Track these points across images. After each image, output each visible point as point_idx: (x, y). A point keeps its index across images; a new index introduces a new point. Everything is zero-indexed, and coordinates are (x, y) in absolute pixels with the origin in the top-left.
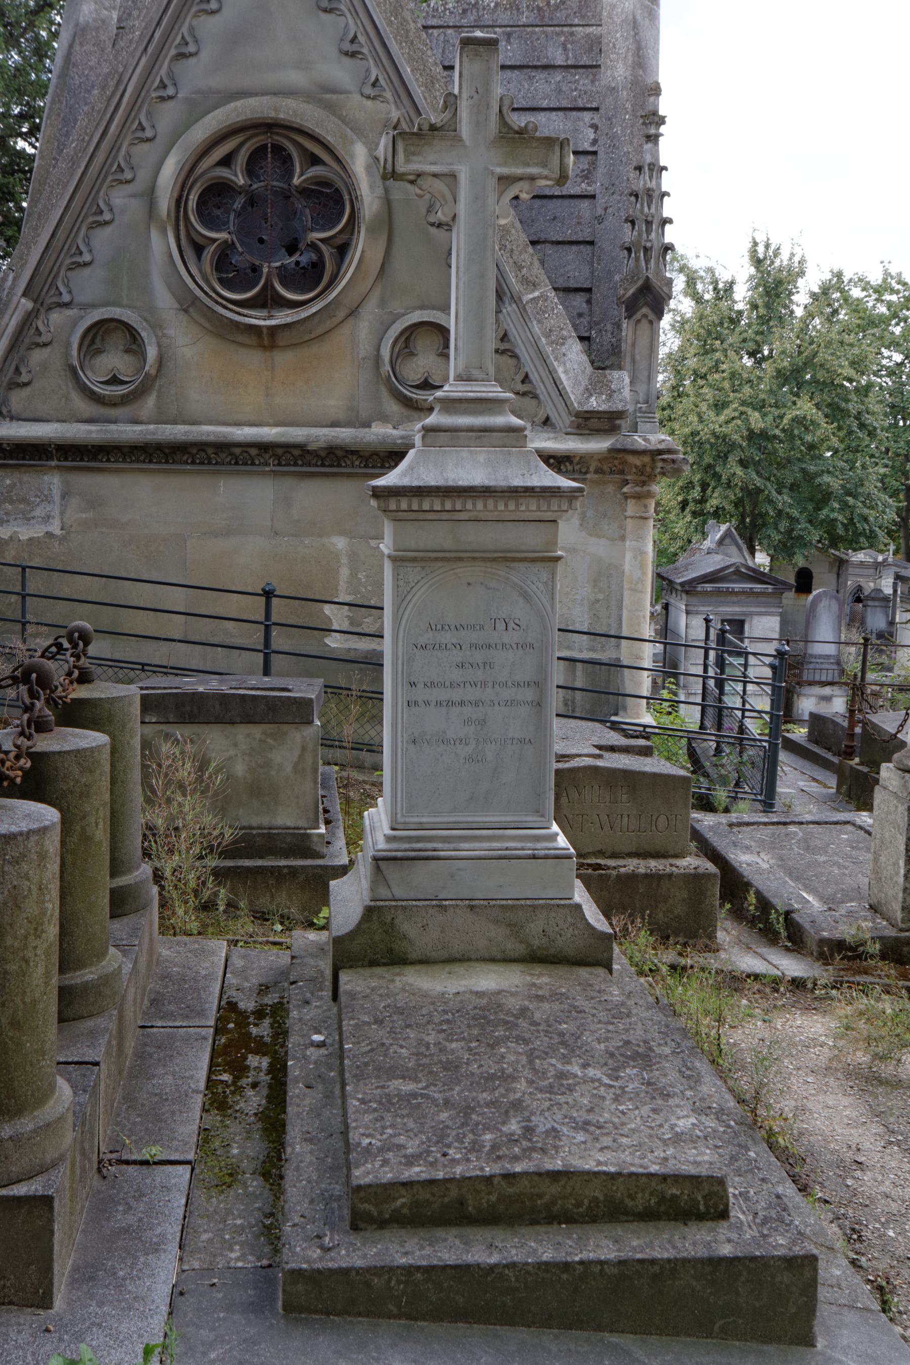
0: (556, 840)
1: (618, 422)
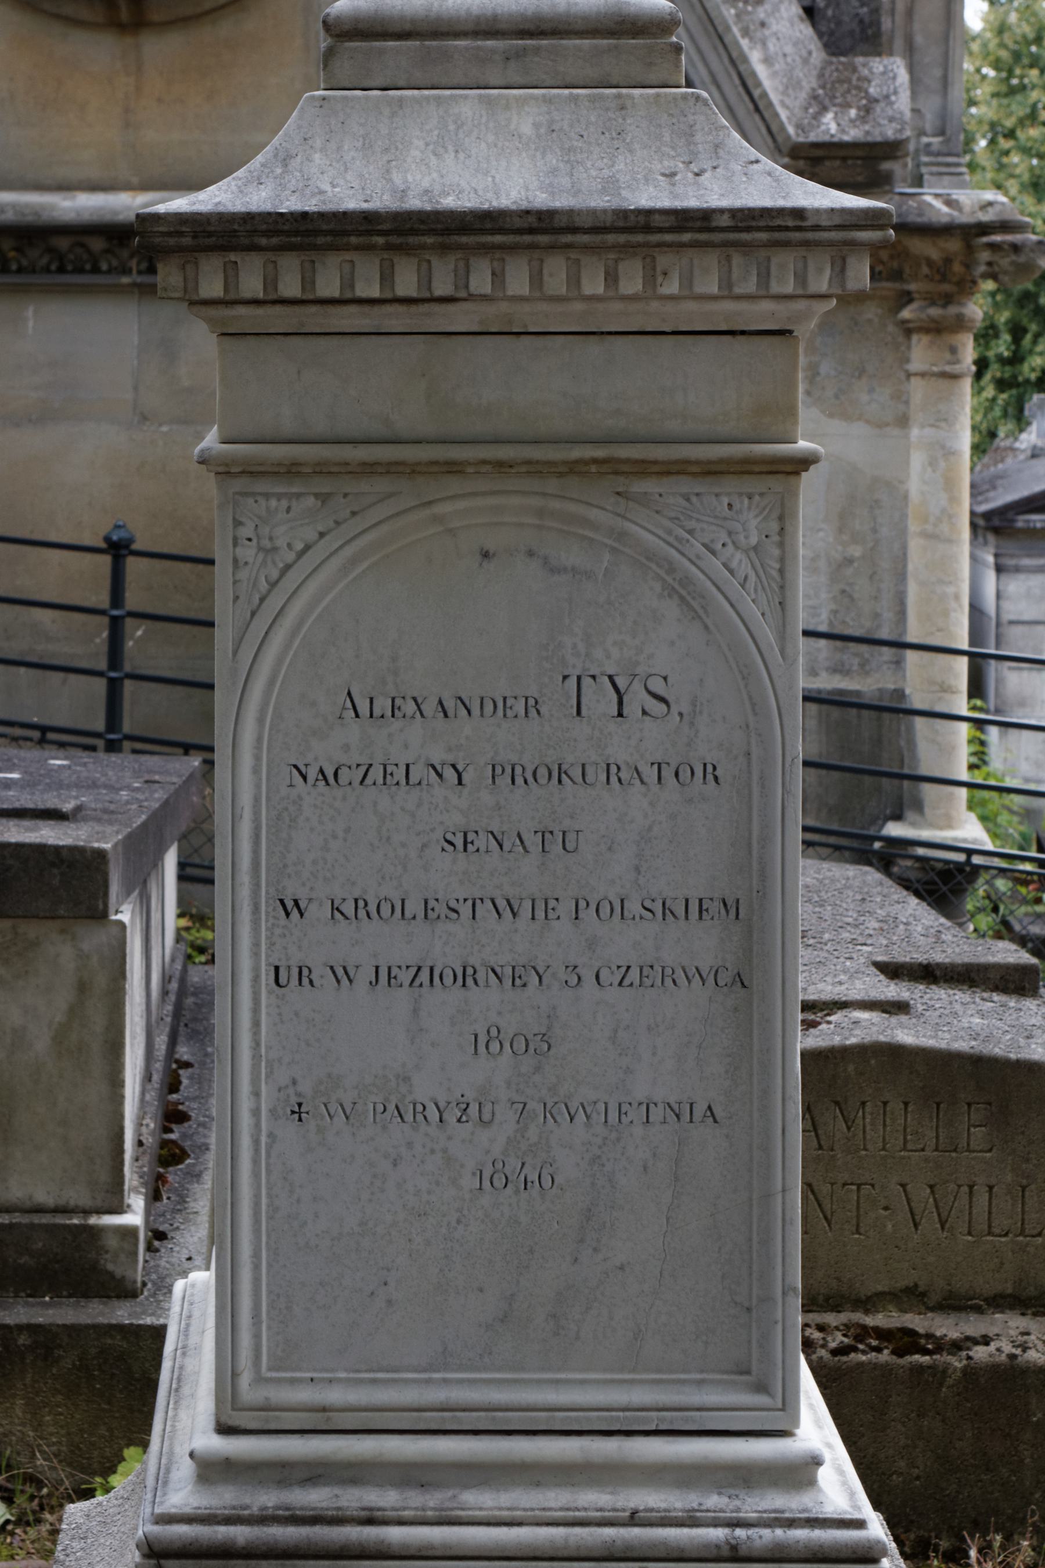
0: (811, 1482)
1: (886, 166)
